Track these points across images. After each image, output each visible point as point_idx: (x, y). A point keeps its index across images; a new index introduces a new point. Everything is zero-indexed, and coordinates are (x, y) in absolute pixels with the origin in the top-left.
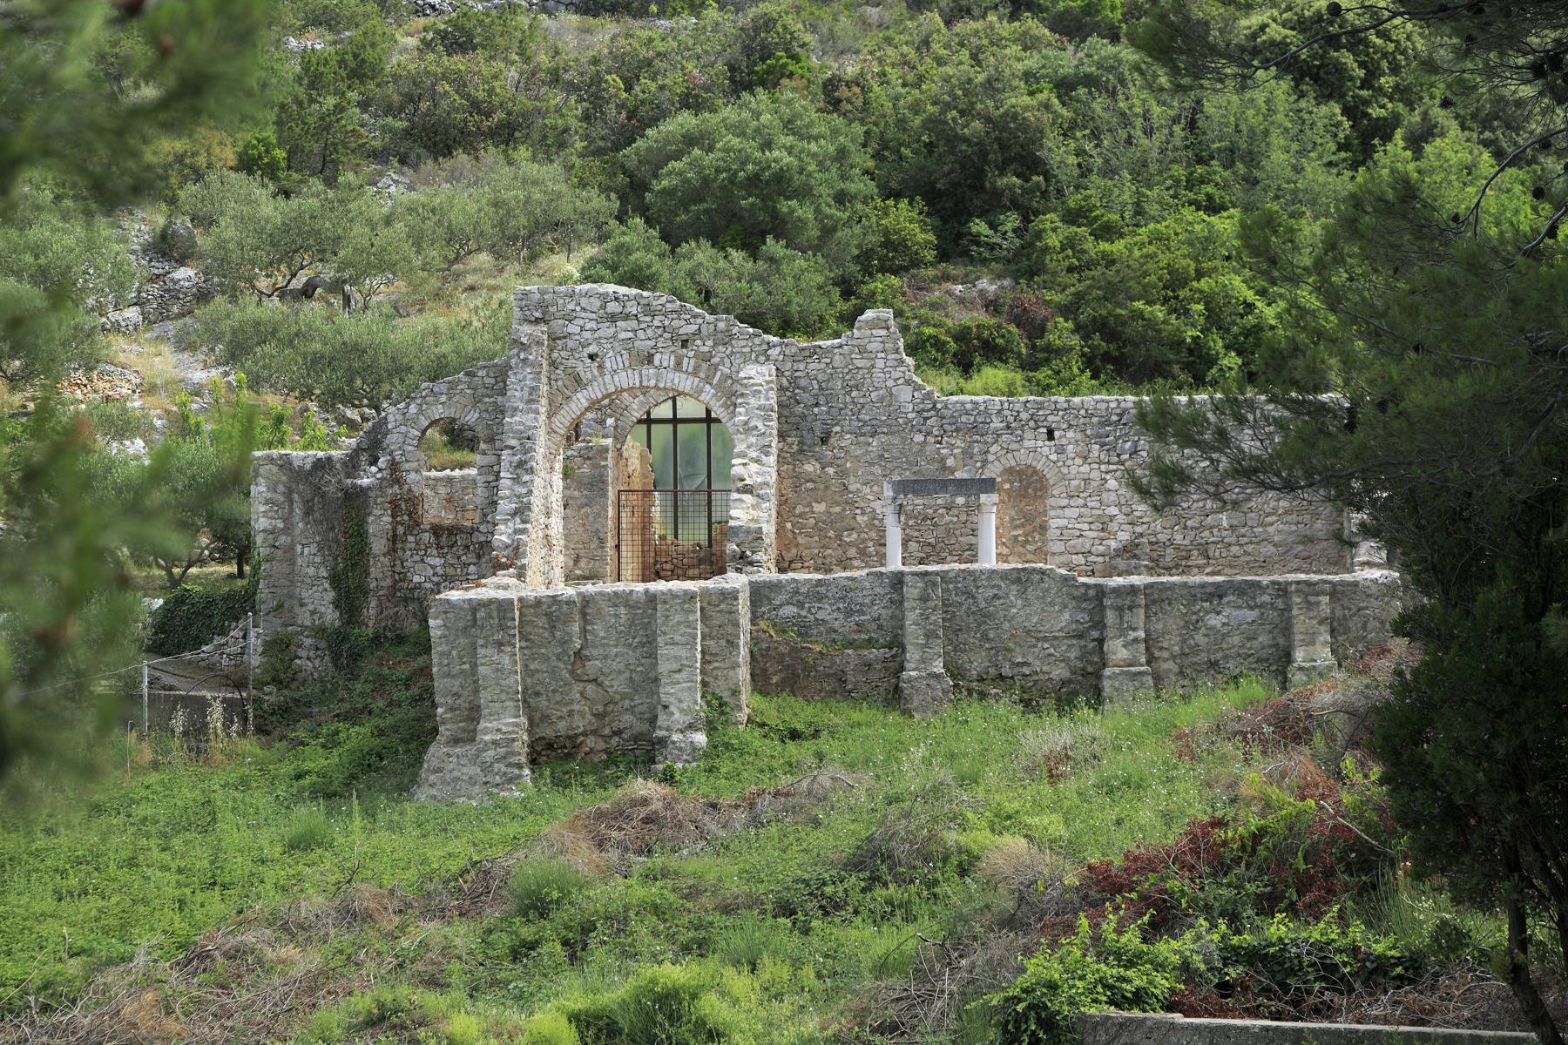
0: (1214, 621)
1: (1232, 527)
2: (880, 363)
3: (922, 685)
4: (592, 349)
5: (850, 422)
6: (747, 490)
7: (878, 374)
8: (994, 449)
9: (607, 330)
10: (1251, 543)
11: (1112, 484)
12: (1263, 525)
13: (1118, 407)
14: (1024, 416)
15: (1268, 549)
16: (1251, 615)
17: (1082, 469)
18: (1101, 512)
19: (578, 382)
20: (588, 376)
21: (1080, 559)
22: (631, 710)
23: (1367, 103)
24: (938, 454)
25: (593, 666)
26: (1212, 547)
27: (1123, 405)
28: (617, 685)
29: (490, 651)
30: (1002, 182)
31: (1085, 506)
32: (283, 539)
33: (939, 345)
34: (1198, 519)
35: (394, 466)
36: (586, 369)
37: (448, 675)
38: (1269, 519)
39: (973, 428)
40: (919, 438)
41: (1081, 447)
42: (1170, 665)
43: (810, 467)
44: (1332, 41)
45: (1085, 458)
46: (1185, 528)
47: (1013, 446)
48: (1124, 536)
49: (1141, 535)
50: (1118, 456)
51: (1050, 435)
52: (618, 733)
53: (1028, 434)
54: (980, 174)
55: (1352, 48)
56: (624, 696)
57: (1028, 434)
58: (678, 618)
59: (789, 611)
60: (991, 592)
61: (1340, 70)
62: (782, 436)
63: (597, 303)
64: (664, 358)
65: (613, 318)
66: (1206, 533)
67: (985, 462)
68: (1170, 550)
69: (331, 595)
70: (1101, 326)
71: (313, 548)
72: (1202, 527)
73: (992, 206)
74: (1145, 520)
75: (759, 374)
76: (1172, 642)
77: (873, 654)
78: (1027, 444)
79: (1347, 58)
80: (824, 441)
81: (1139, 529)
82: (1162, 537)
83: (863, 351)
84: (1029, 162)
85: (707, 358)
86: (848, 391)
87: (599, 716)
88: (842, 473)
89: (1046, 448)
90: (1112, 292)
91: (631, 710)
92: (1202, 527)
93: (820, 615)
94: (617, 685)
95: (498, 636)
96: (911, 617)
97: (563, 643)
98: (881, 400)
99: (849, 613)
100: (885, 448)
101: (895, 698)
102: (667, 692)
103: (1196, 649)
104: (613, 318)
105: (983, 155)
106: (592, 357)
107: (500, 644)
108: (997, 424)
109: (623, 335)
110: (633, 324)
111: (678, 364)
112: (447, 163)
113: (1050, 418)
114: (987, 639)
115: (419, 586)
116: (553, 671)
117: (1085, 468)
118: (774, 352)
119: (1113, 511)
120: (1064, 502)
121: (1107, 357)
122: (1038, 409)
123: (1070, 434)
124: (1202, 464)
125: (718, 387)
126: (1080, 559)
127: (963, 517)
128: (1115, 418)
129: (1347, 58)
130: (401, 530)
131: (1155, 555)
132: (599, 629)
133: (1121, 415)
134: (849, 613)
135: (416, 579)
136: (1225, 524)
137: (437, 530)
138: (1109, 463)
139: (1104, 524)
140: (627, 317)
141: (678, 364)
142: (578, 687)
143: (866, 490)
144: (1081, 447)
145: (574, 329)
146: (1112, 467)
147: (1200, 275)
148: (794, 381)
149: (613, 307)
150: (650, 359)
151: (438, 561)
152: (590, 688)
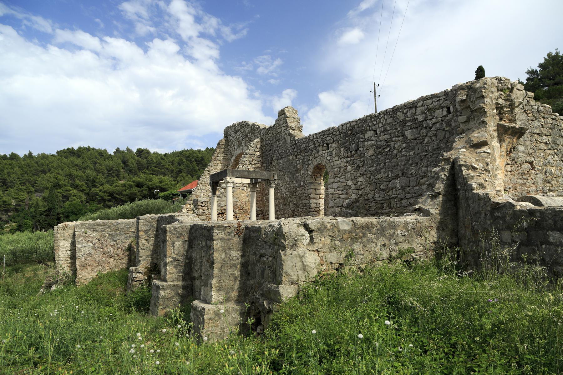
1: (403, 188)
8: (311, 157)
10: (412, 197)
12: (418, 184)
13: (350, 126)
17: (338, 162)
18: (345, 184)
24: (296, 163)
26: (392, 201)
27: (352, 125)
31: (340, 181)
34: (385, 184)
38: (423, 181)
45: (339, 156)
46: (380, 190)
47: (316, 155)
48: (354, 197)
49: (361, 196)
50: (351, 152)
51: (328, 144)
66: (390, 193)
67: (309, 165)
68: (373, 204)
72: (388, 189)
74: (362, 187)
78: (320, 153)
81: (360, 192)
82: (370, 196)
98: (283, 143)
113: (328, 138)
117: (339, 162)
119: (350, 183)
120: (332, 180)
122: (323, 135)
123: (334, 145)
124: (386, 150)
127: (303, 191)
128: (349, 132)
131: (367, 206)
133: (352, 130)
136: (398, 186)
138: (348, 157)
146: (349, 159)
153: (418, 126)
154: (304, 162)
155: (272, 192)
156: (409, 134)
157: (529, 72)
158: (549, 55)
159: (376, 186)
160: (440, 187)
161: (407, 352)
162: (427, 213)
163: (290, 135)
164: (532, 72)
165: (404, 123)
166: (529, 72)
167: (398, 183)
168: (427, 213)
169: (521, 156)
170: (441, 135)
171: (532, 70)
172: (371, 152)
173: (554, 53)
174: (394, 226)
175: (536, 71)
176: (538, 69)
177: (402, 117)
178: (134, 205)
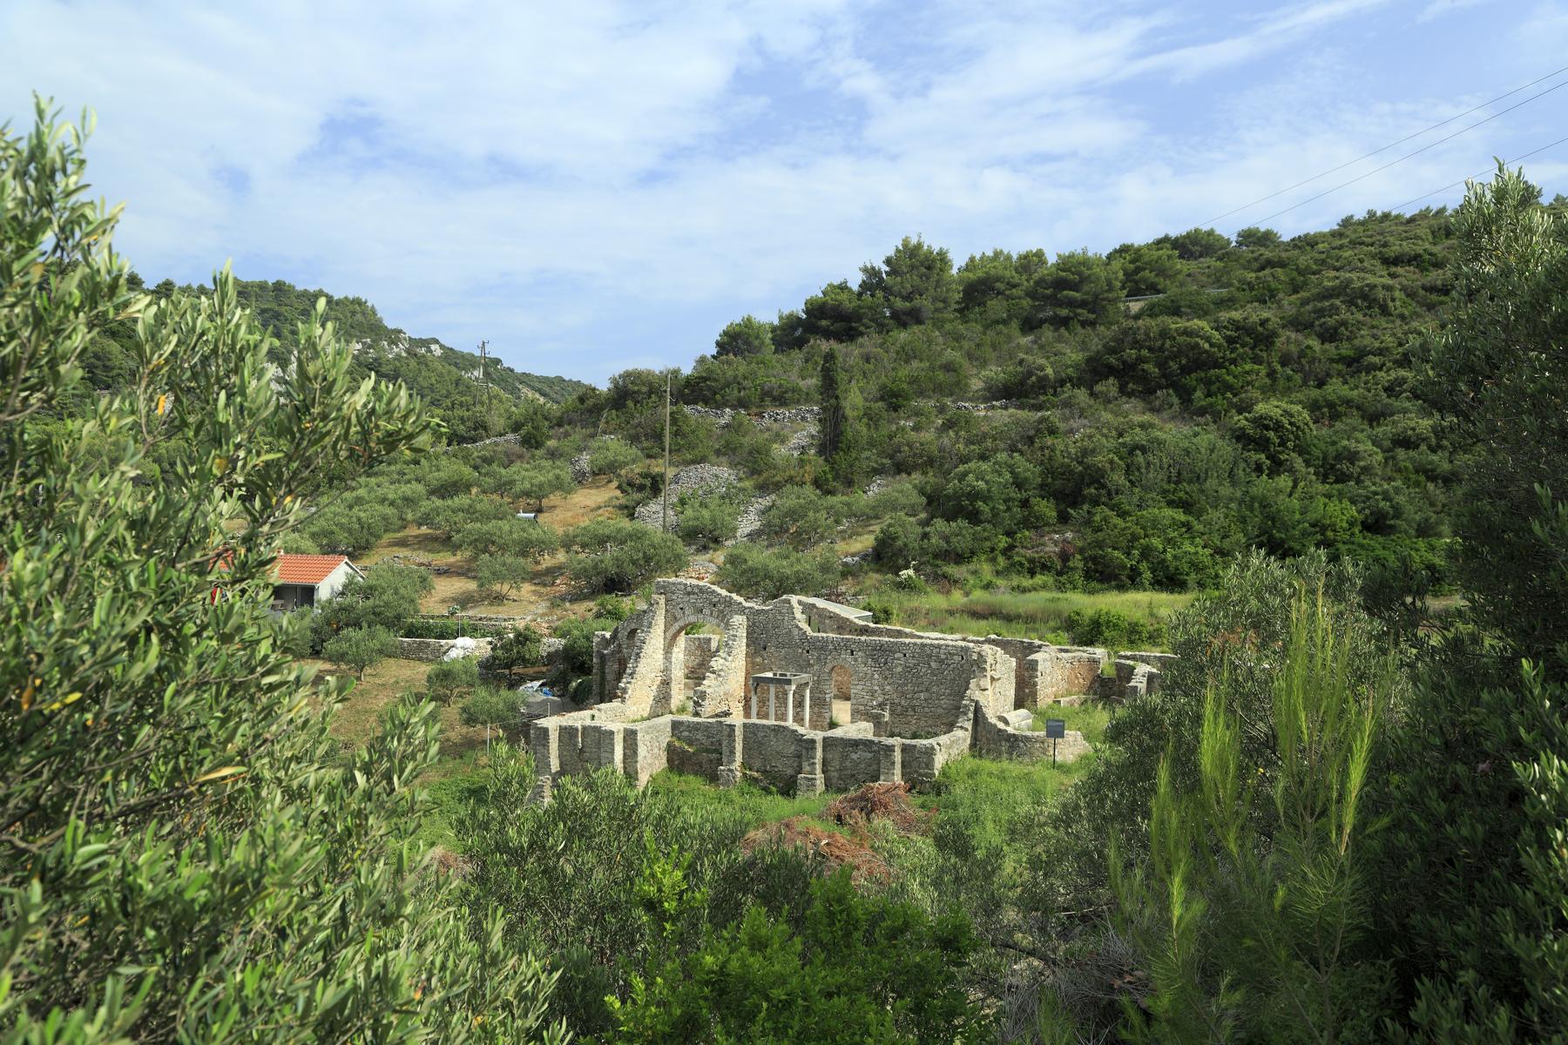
0: (854, 756)
3: (724, 774)
6: (714, 672)
11: (876, 676)
15: (940, 711)
16: (870, 755)
19: (675, 618)
21: (862, 708)
23: (1279, 452)
30: (1086, 492)
33: (1021, 565)
36: (679, 614)
42: (836, 774)
43: (758, 660)
44: (1267, 428)
48: (880, 699)
55: (1276, 430)
59: (686, 734)
61: (1268, 440)
62: (748, 645)
65: (689, 594)
70: (1094, 559)
72: (913, 698)
76: (836, 764)
79: (1271, 434)
86: (774, 628)
89: (849, 658)
90: (1100, 545)
92: (913, 698)
99: (708, 737)
100: (787, 654)
103: (845, 768)
104: (689, 594)
112: (898, 478)
114: (760, 754)
116: (571, 756)
121: (1096, 571)
126: (862, 708)
129: (1271, 434)
134: (708, 737)
139: (873, 693)
147: (1146, 536)
148: (754, 623)
149: (689, 589)
153: (942, 662)
154: (819, 659)
155: (808, 691)
156: (933, 664)
157: (865, 270)
158: (906, 243)
159: (903, 694)
160: (971, 715)
161: (1520, 278)
162: (966, 730)
163: (797, 626)
164: (871, 272)
165: (930, 656)
166: (865, 270)
167: (922, 696)
168: (966, 730)
169: (997, 690)
170: (957, 672)
171: (873, 268)
172: (899, 669)
173: (914, 241)
174: (428, 645)
175: (880, 272)
176: (885, 268)
178: (536, 669)
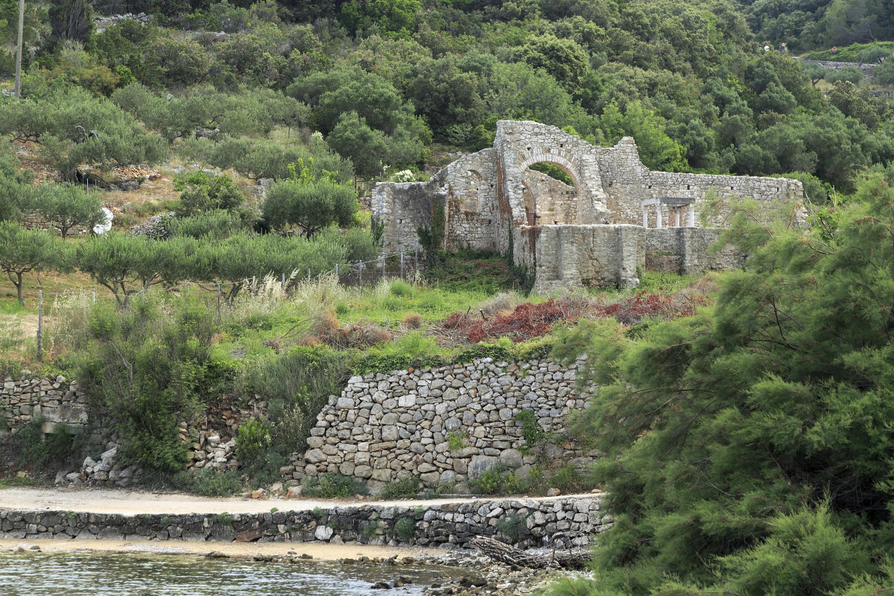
2: (630, 157)
4: (529, 146)
5: (620, 179)
7: (629, 161)
9: (534, 139)
14: (680, 180)
19: (524, 158)
20: (527, 156)
22: (608, 271)
25: (596, 254)
28: (603, 261)
29: (569, 245)
32: (391, 217)
35: (450, 188)
36: (526, 153)
37: (547, 255)
39: (662, 184)
40: (643, 186)
41: (699, 193)
51: (688, 187)
52: (603, 279)
53: (681, 187)
54: (446, 106)
56: (606, 265)
57: (681, 187)
58: (631, 236)
60: (709, 237)
63: (531, 128)
64: (554, 151)
69: (418, 239)
71: (408, 220)
73: (454, 119)
75: (590, 158)
77: (673, 258)
79: (567, 67)
80: (610, 185)
83: (624, 152)
84: (467, 102)
85: (569, 151)
87: (597, 272)
88: (617, 198)
91: (608, 271)
93: (653, 243)
94: (603, 261)
95: (572, 240)
96: (688, 244)
97: (587, 244)
99: (662, 242)
101: (681, 271)
102: (626, 264)
104: (536, 134)
105: (447, 99)
106: (529, 149)
107: (572, 243)
108: (670, 182)
109: (540, 141)
110: (543, 137)
111: (559, 153)
115: (459, 235)
118: (593, 151)
125: (573, 163)
130: (452, 213)
132: (598, 240)
134: (662, 242)
135: (458, 232)
137: (467, 214)
140: (541, 134)
141: (559, 153)
142: (591, 261)
143: (625, 205)
144: (699, 193)
145: (522, 138)
149: (536, 130)
150: (549, 151)
151: (467, 226)
152: (595, 261)
156: (755, 195)
165: (753, 189)
177: (752, 185)
